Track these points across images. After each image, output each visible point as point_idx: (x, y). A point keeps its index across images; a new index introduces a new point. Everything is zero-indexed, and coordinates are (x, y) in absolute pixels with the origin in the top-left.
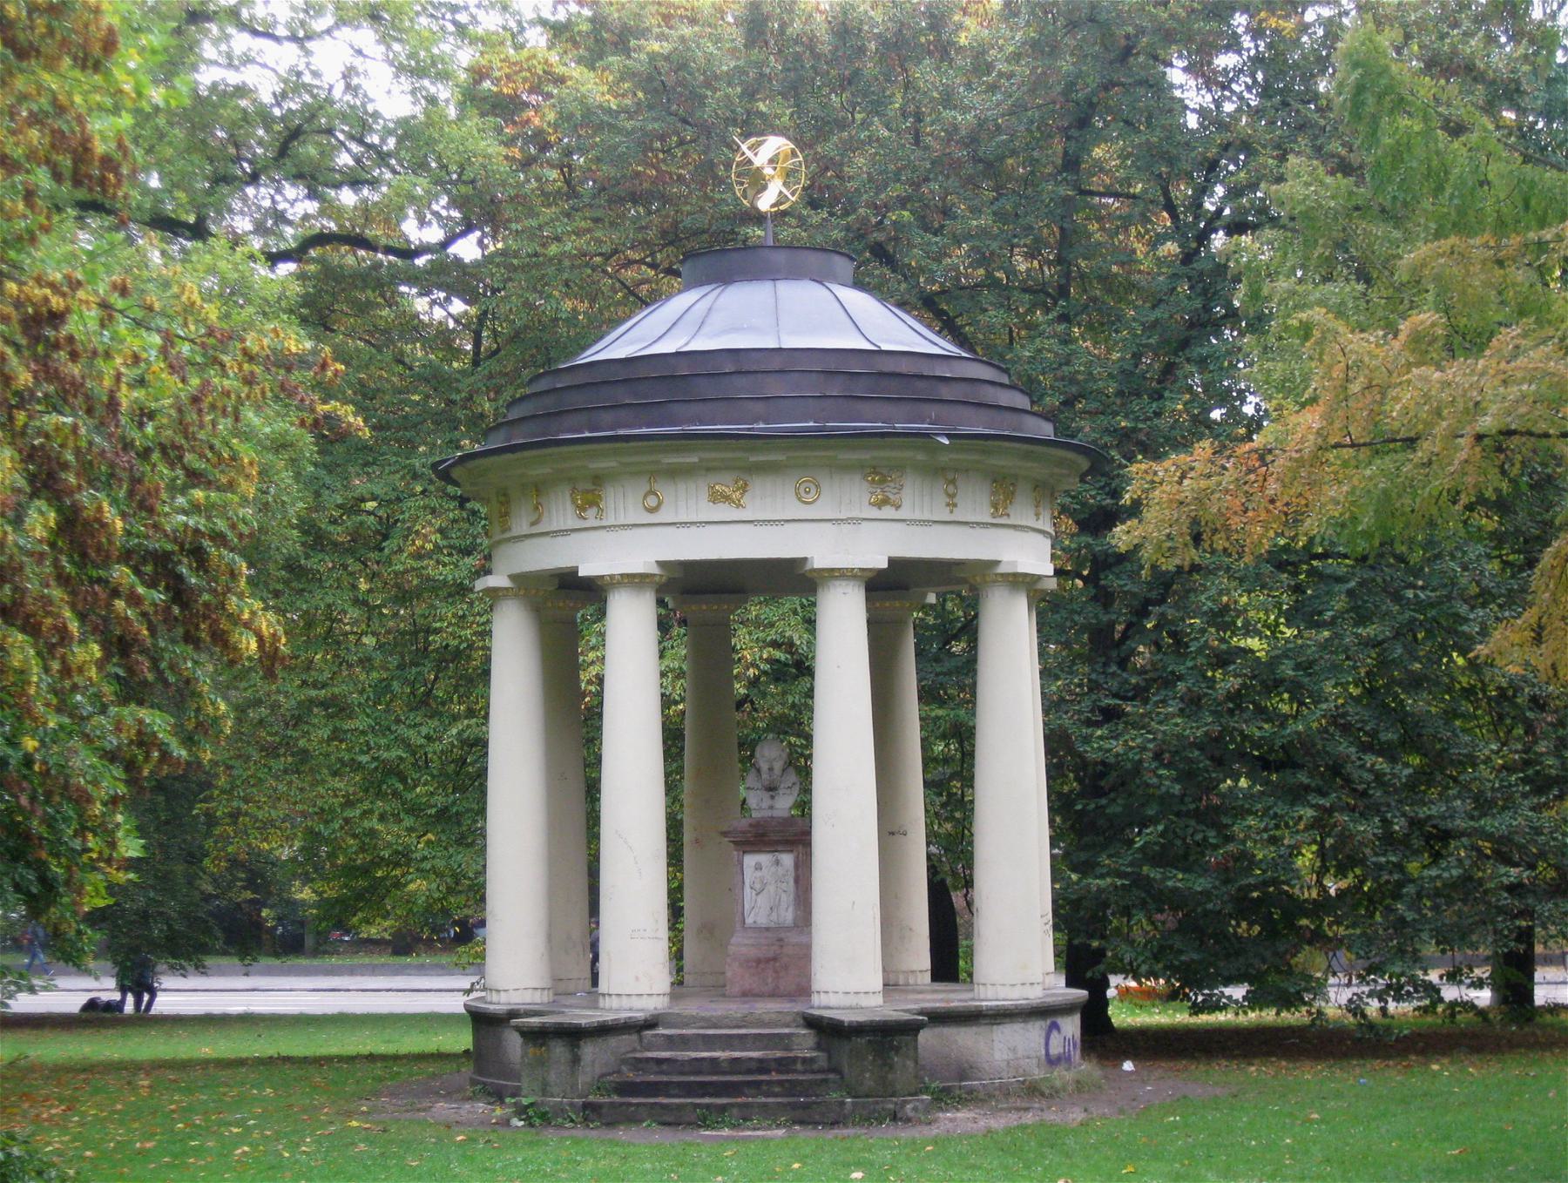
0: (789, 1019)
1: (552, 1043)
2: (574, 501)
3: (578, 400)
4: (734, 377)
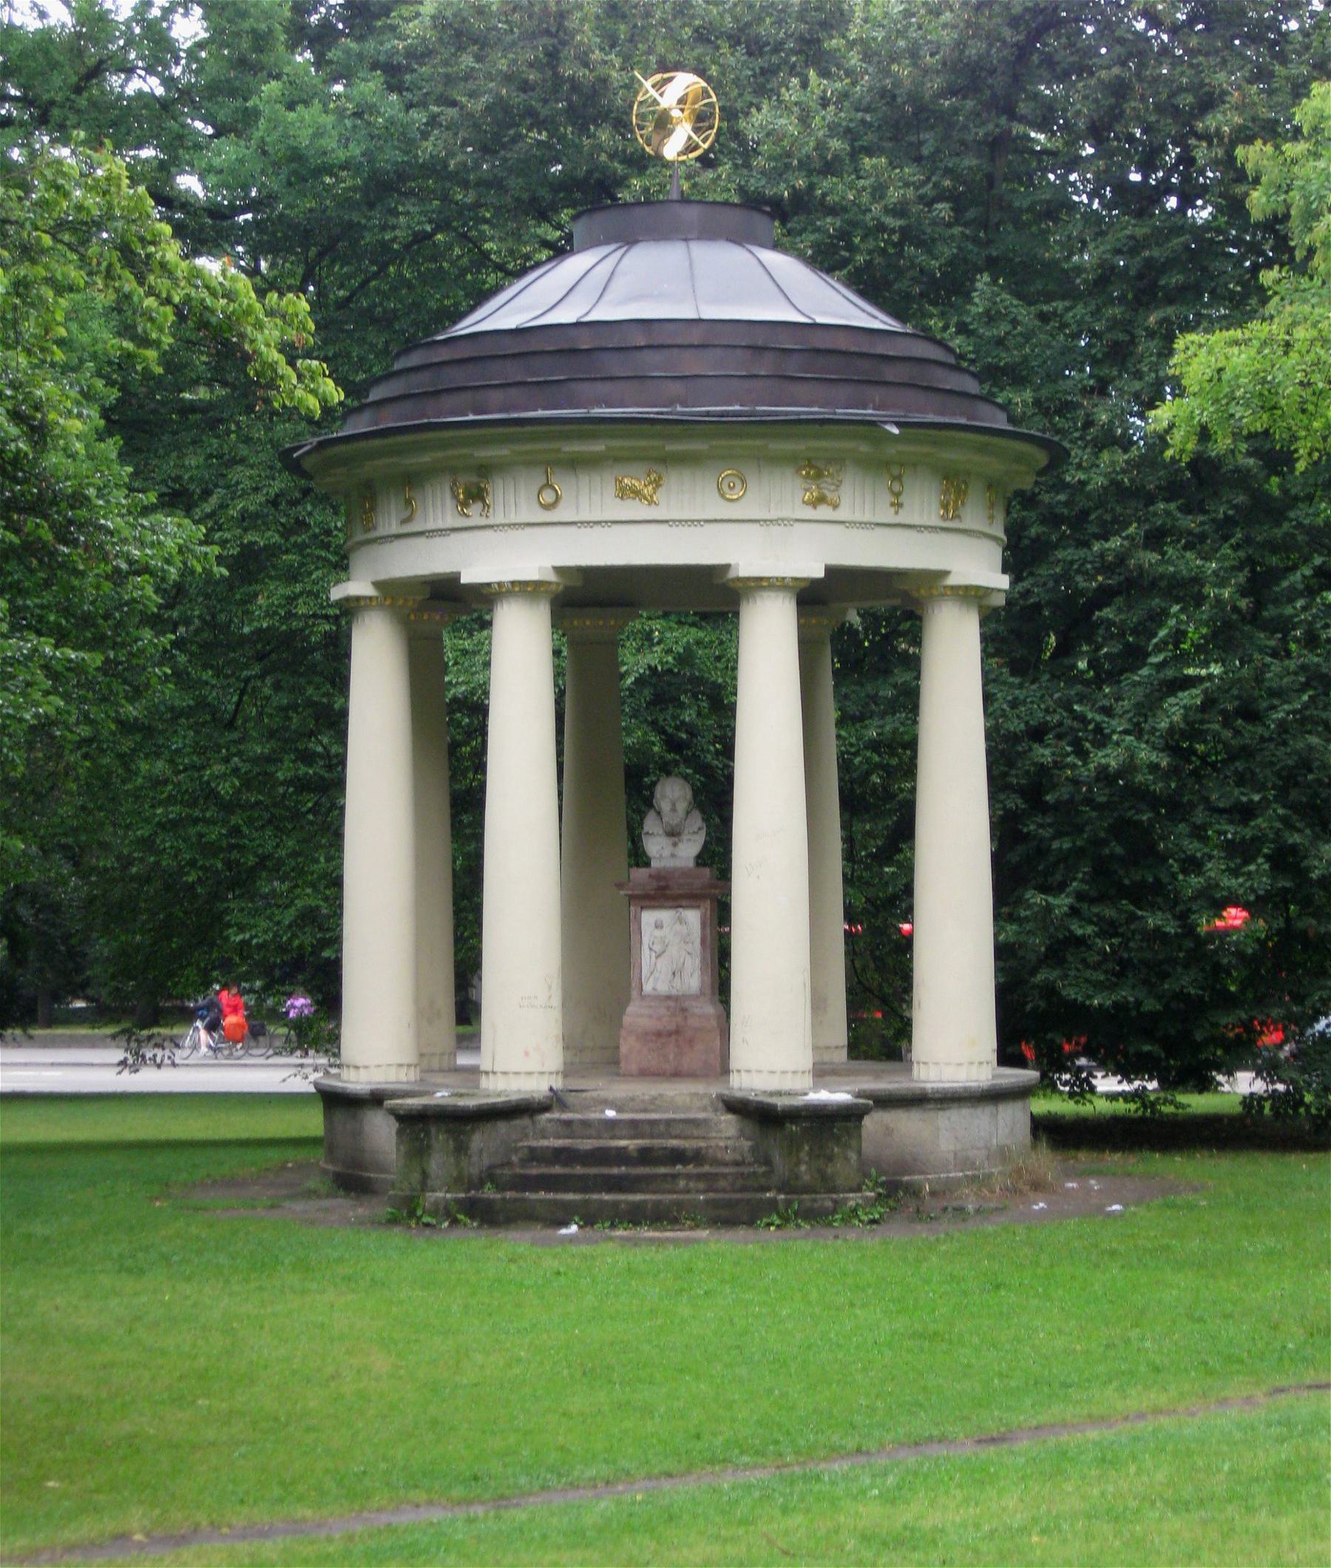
2: (455, 496)
3: (457, 376)
4: (646, 352)
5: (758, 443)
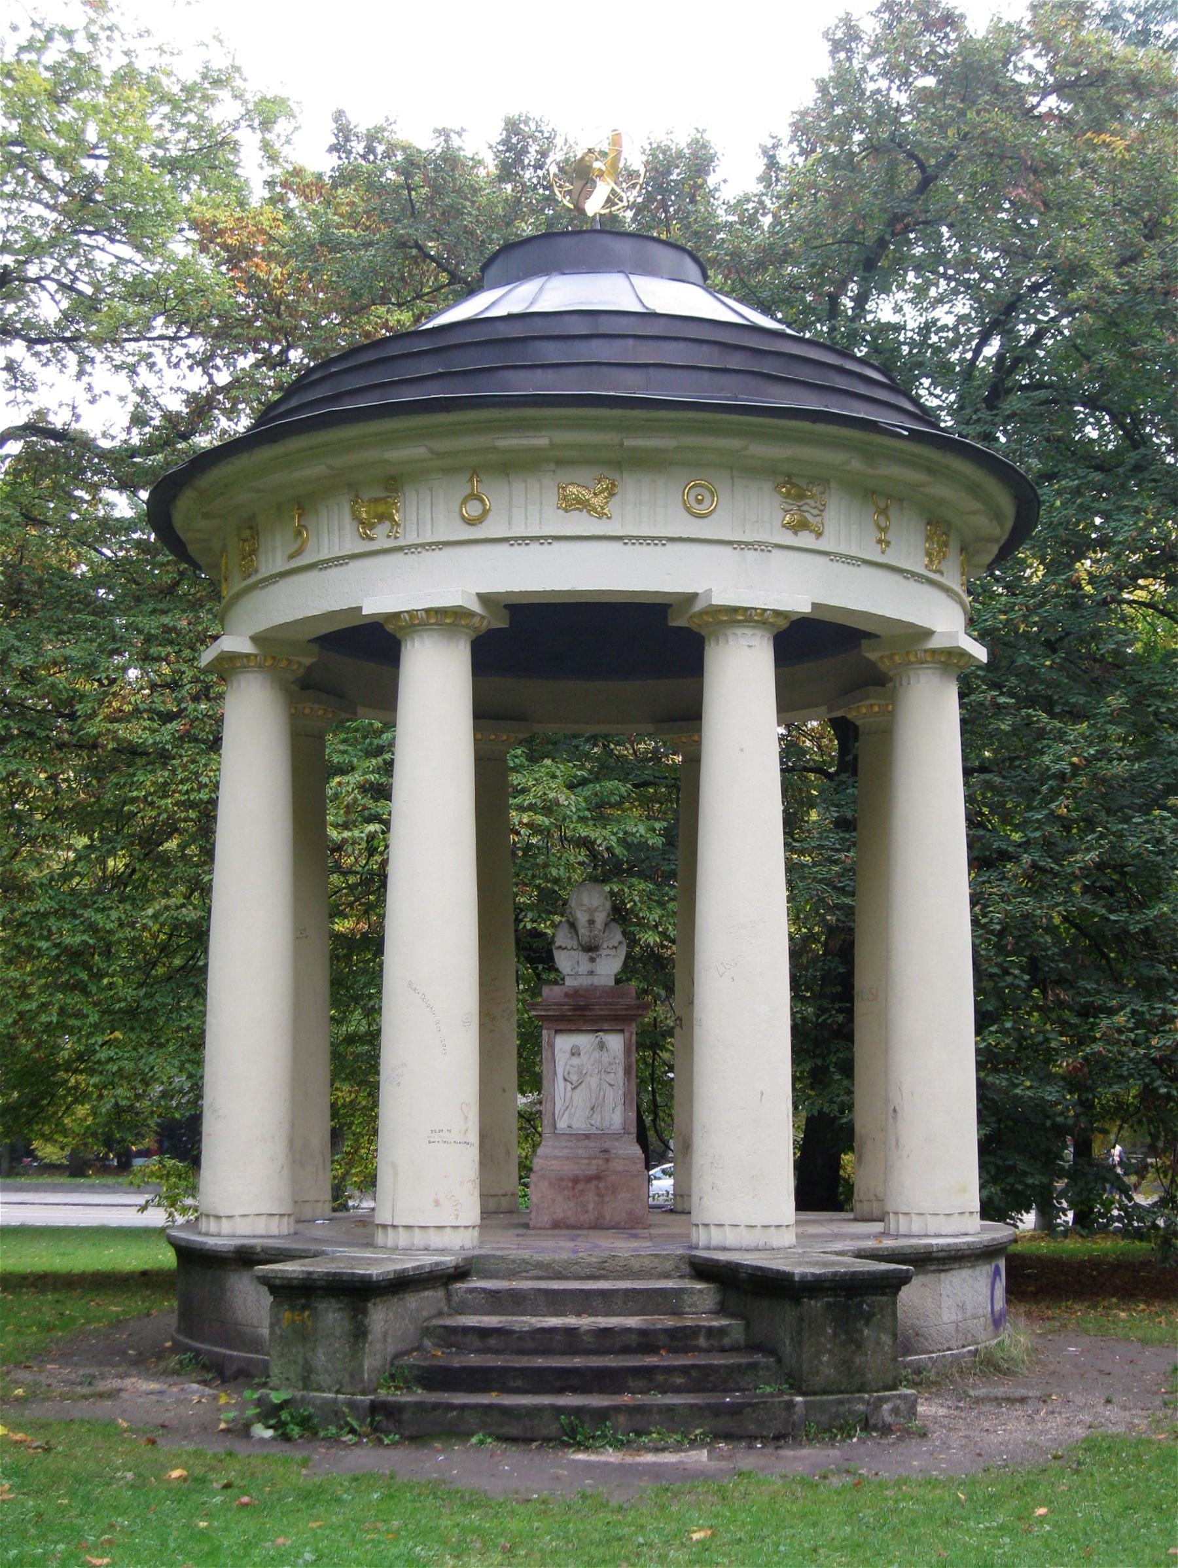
0: (669, 1265)
1: (322, 1306)
5: (735, 443)
